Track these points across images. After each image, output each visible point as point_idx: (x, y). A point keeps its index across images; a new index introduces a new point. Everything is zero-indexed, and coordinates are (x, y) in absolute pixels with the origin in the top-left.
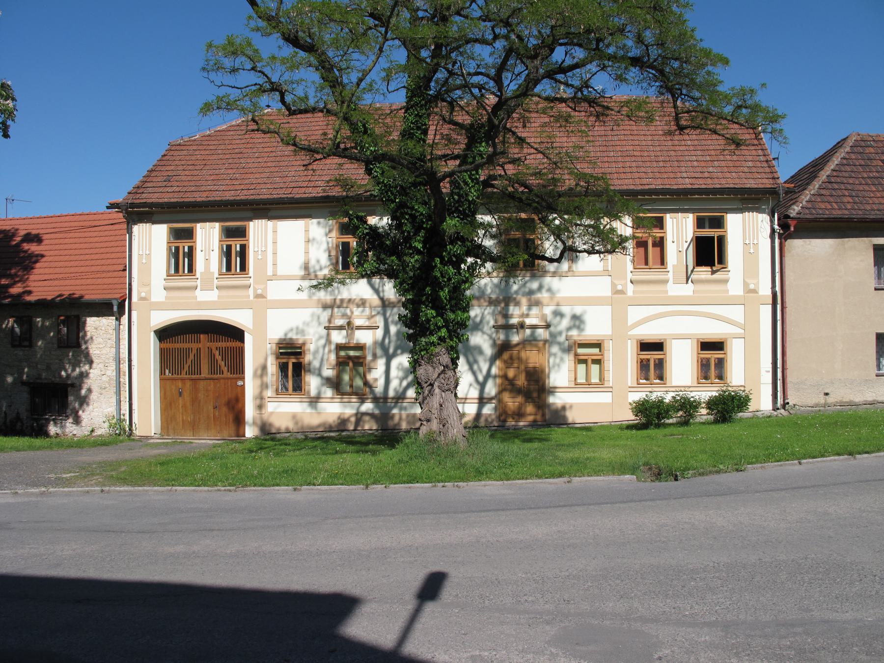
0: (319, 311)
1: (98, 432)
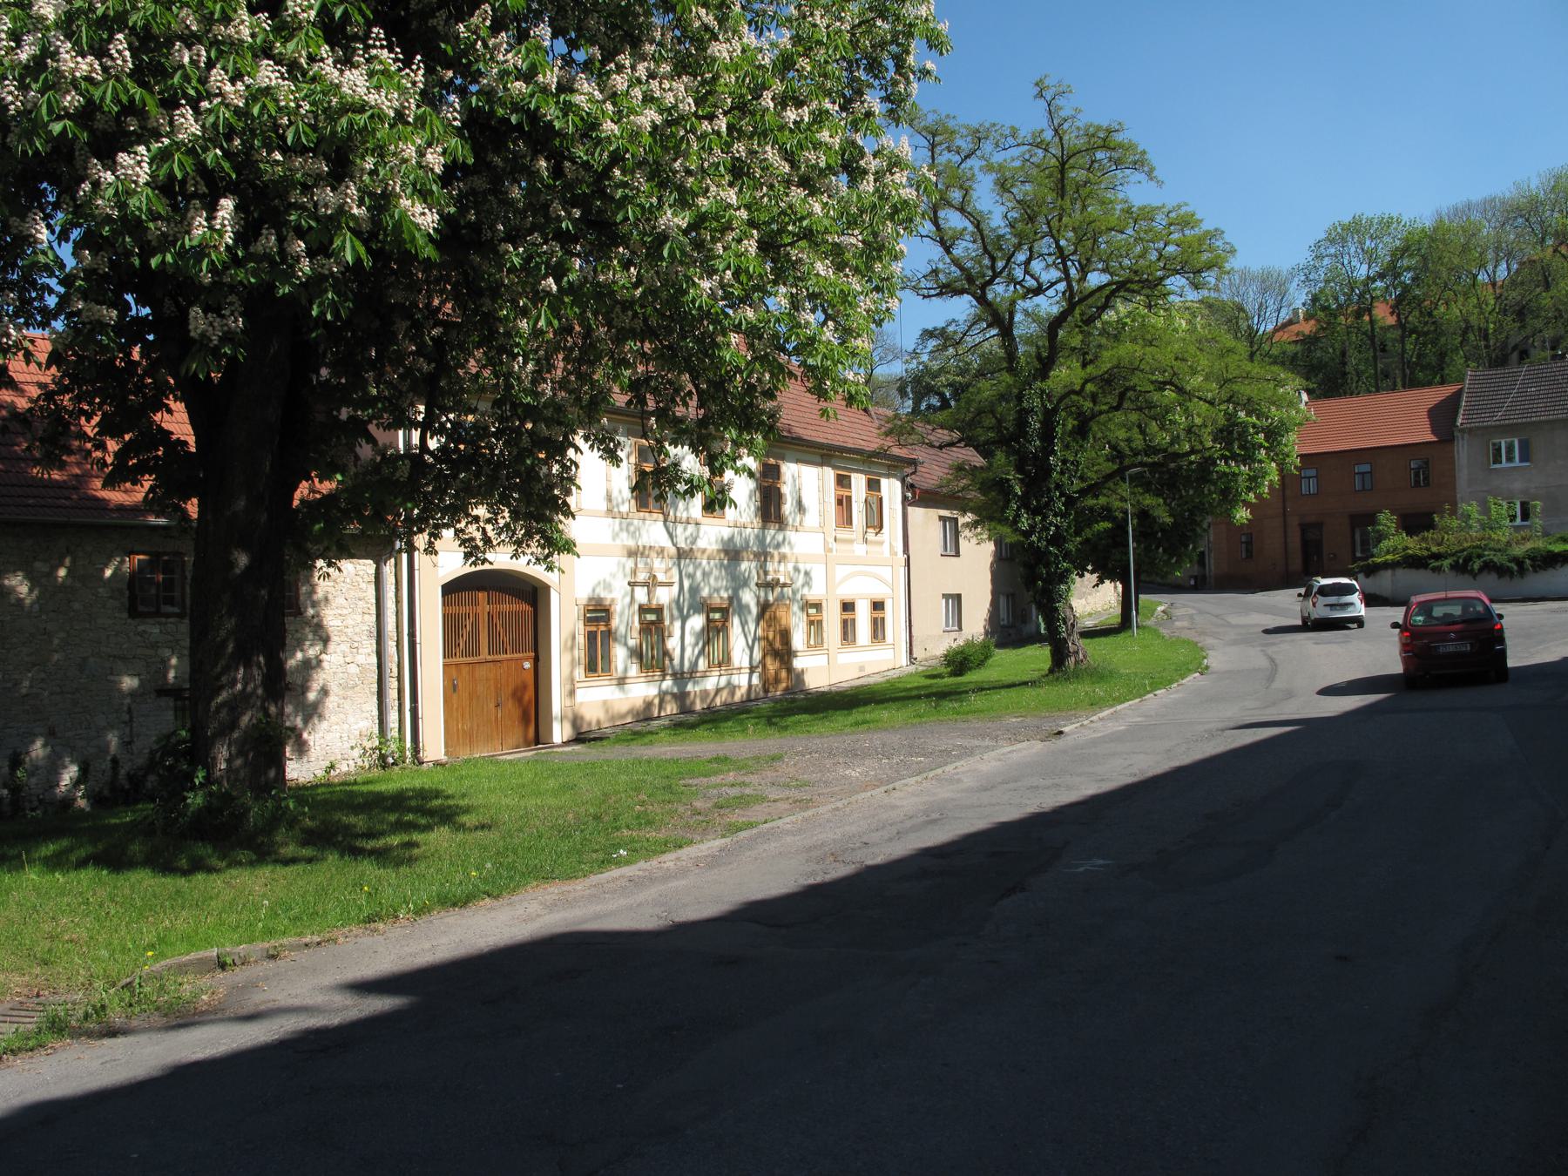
0: (624, 560)
1: (343, 768)
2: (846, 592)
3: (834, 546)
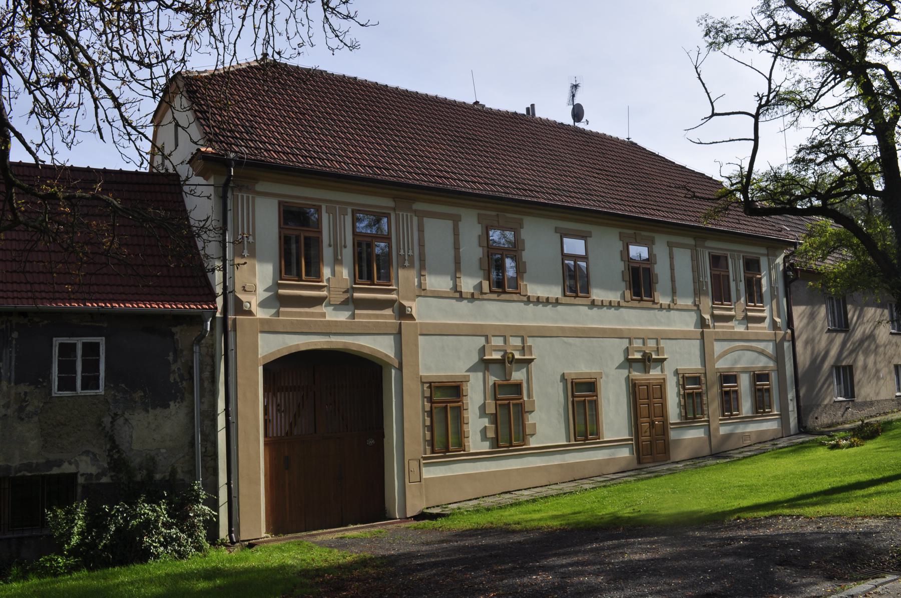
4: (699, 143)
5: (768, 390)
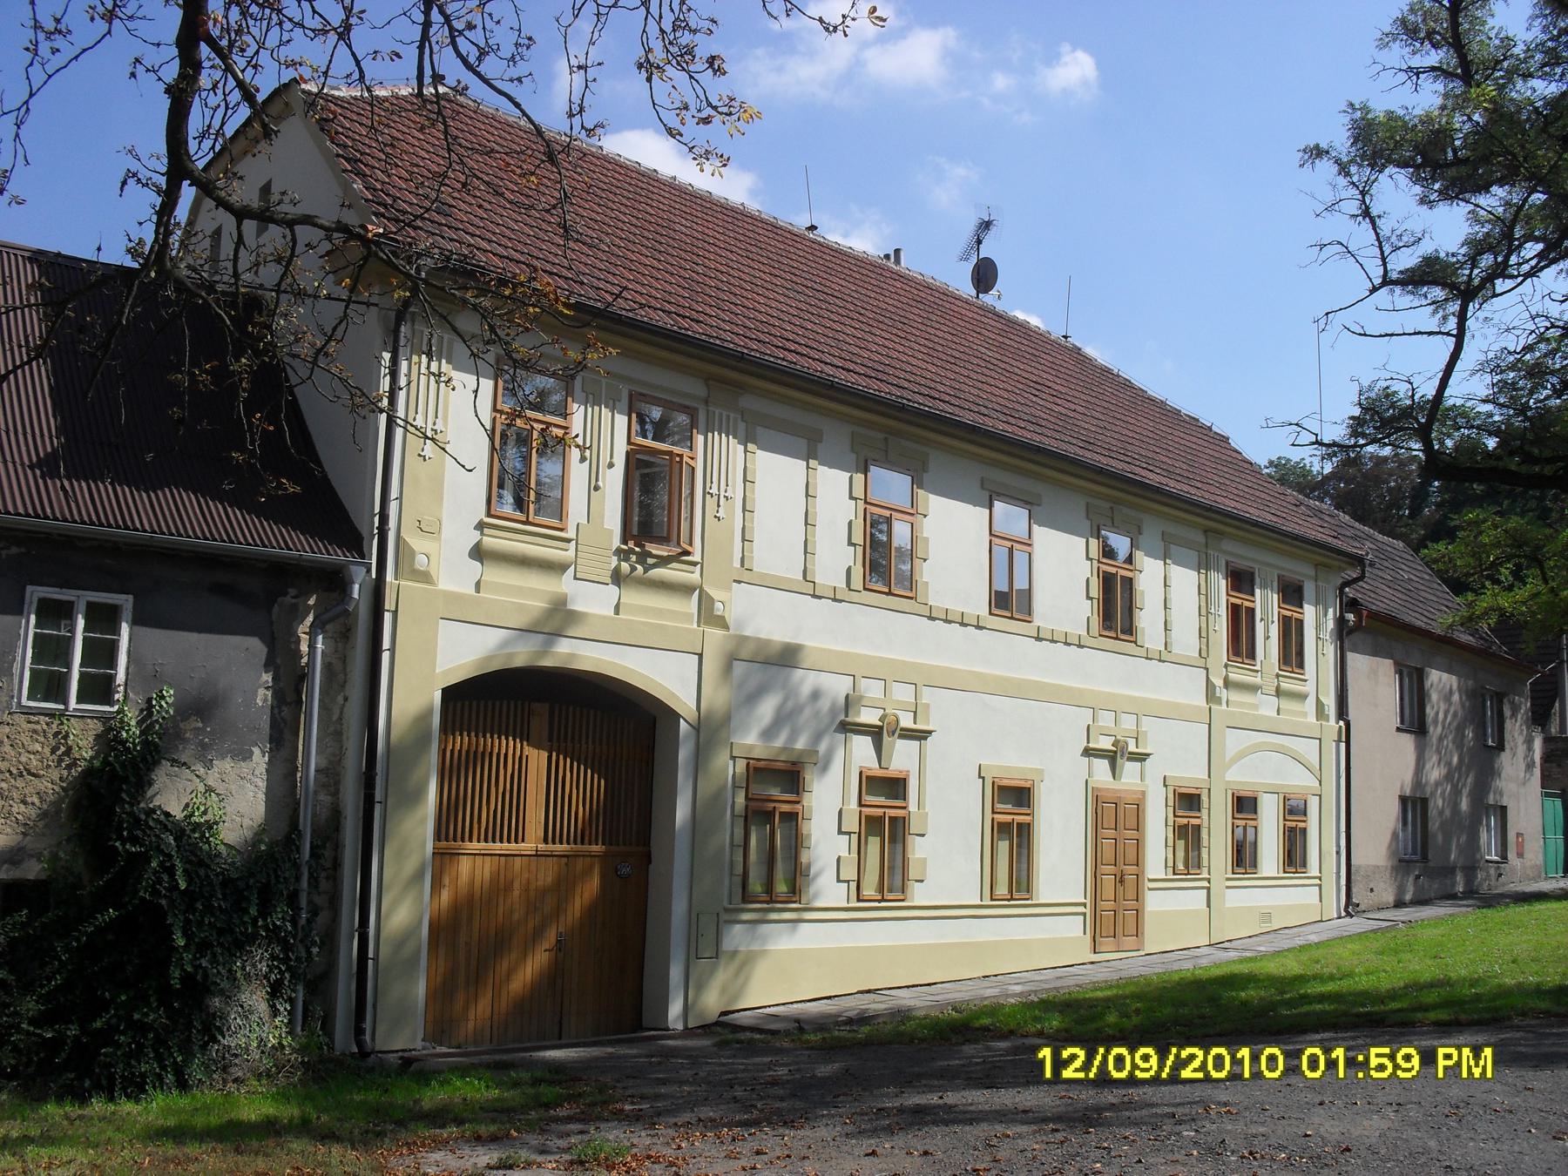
2: (1241, 776)
3: (1223, 694)
4: (1360, 334)
5: (1304, 831)
